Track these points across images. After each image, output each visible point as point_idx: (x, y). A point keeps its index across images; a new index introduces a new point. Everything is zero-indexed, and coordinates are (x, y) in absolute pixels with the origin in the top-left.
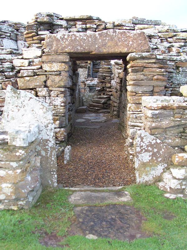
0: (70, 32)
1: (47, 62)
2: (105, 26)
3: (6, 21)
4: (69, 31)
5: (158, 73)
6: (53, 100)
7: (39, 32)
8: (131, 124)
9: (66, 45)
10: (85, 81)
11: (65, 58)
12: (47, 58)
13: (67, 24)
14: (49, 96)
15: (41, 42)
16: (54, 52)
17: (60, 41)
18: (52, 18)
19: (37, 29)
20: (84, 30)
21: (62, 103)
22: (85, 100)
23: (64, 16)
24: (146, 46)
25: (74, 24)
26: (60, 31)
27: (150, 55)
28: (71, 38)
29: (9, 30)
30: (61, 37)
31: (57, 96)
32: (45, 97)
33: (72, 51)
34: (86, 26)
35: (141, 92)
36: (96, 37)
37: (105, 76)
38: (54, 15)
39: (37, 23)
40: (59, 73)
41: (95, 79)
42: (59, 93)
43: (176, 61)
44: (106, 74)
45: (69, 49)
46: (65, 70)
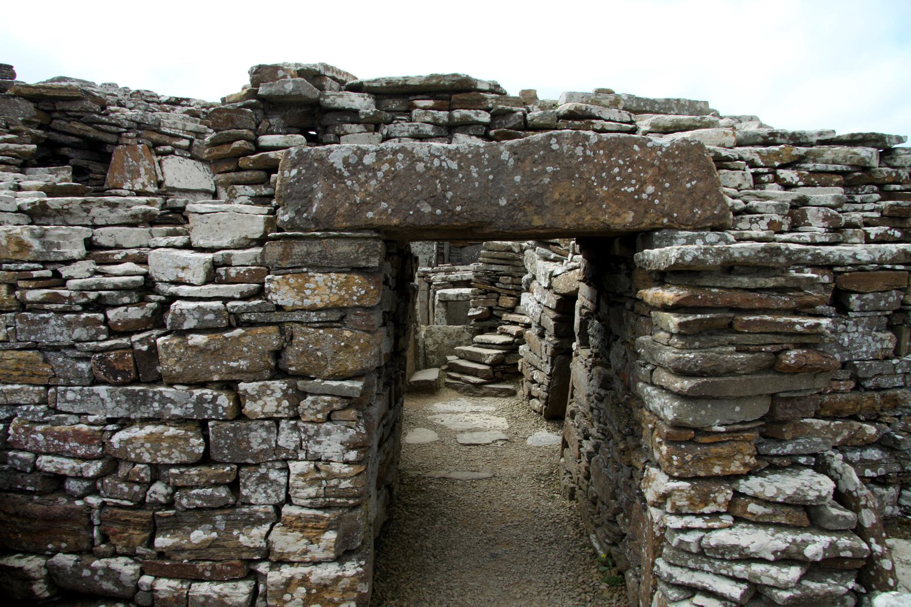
0: (386, 138)
1: (280, 270)
2: (525, 115)
3: (182, 99)
4: (385, 132)
5: (798, 340)
6: (310, 437)
7: (262, 138)
8: (670, 576)
9: (370, 195)
10: (428, 272)
11: (364, 251)
12: (285, 248)
13: (377, 107)
14: (291, 419)
15: (269, 177)
16: (317, 225)
17: (341, 176)
18: (317, 82)
19: (257, 126)
20: (444, 132)
21: (348, 449)
22: (432, 348)
23: (365, 73)
24: (714, 204)
25: (403, 108)
26: (346, 133)
27: (762, 255)
28: (392, 163)
29: (188, 128)
30: (345, 161)
31: (329, 419)
32: (277, 421)
33: (395, 221)
34: (450, 117)
35: (723, 429)
36: (504, 163)
37: (495, 272)
38: (329, 74)
39: (254, 101)
40: (337, 316)
41: (457, 267)
42: (335, 406)
43: (838, 269)
44: (500, 268)
45: (381, 214)
46: (366, 303)
